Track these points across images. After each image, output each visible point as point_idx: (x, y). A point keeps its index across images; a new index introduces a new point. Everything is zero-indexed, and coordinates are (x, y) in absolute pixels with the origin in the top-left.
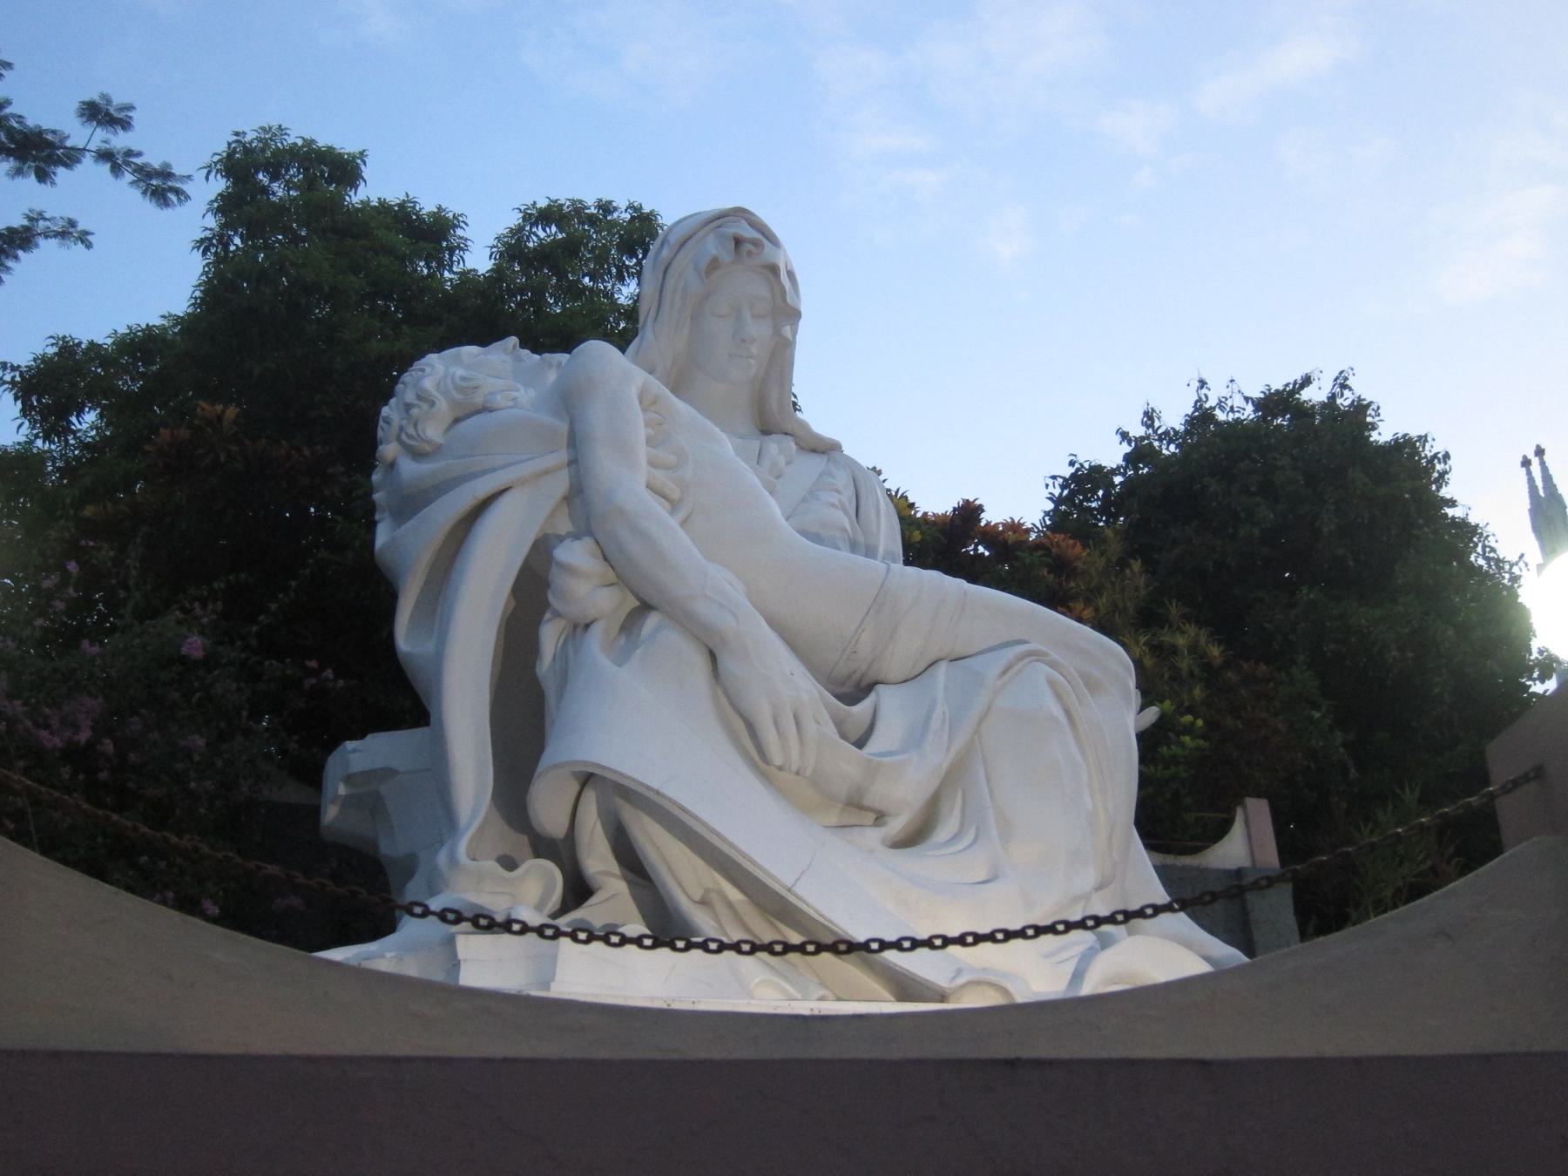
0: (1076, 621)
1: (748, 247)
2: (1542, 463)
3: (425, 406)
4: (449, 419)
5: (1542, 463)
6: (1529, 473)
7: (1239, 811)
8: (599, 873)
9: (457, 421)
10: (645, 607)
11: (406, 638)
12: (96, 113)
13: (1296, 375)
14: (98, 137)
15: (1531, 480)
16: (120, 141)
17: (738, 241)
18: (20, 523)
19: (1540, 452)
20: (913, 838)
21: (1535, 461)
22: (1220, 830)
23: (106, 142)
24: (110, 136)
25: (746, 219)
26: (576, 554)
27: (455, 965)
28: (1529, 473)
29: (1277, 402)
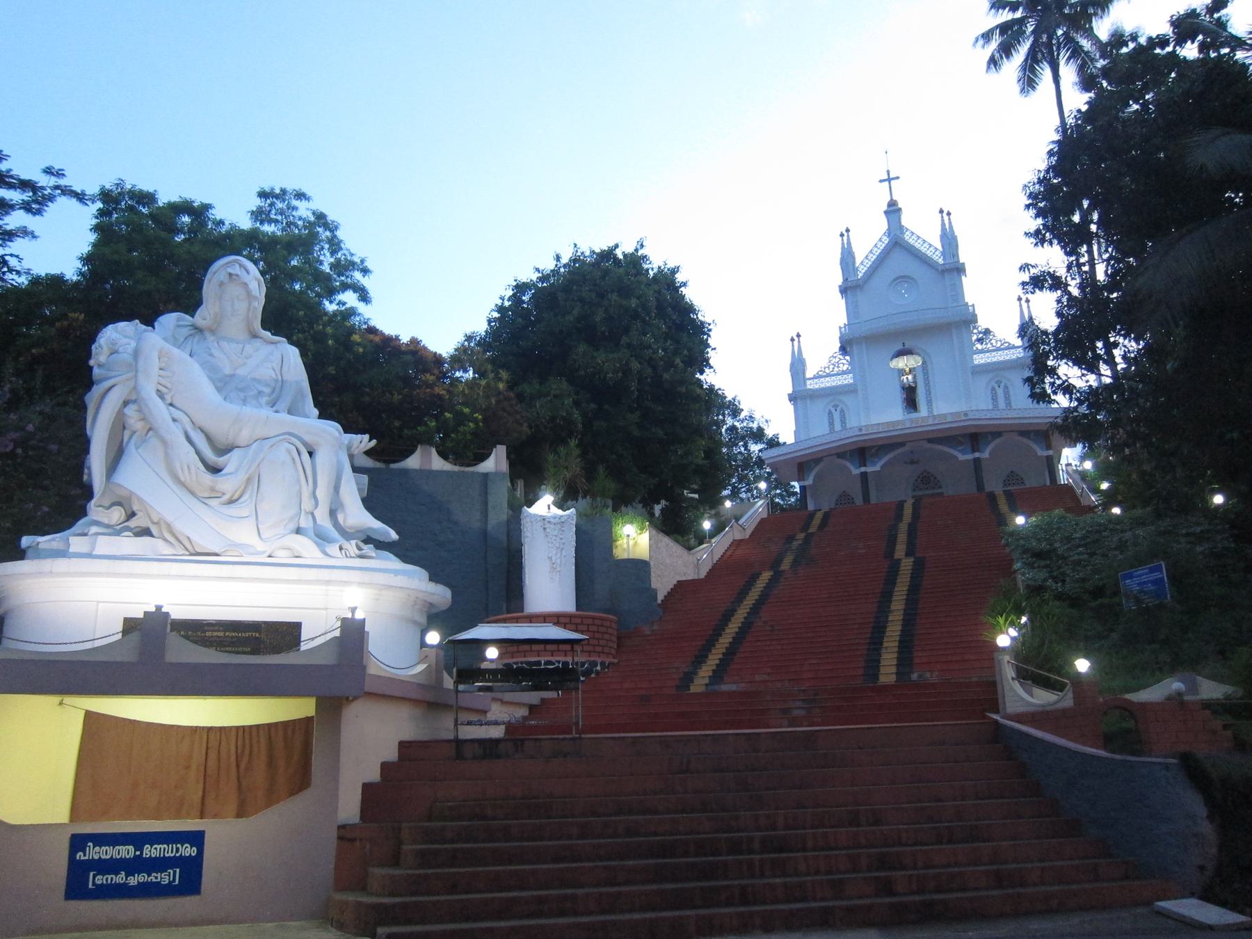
0: (226, 454)
1: (234, 277)
2: (848, 236)
3: (100, 349)
4: (109, 353)
5: (848, 236)
6: (843, 240)
7: (494, 449)
8: (137, 510)
9: (112, 354)
10: (150, 429)
11: (88, 433)
12: (48, 171)
13: (611, 244)
14: (53, 181)
15: (843, 244)
16: (62, 182)
17: (230, 275)
18: (174, 238)
19: (848, 230)
20: (231, 502)
21: (846, 234)
22: (483, 457)
23: (56, 182)
24: (58, 180)
25: (239, 263)
26: (130, 411)
27: (69, 545)
28: (843, 240)
29: (608, 255)
